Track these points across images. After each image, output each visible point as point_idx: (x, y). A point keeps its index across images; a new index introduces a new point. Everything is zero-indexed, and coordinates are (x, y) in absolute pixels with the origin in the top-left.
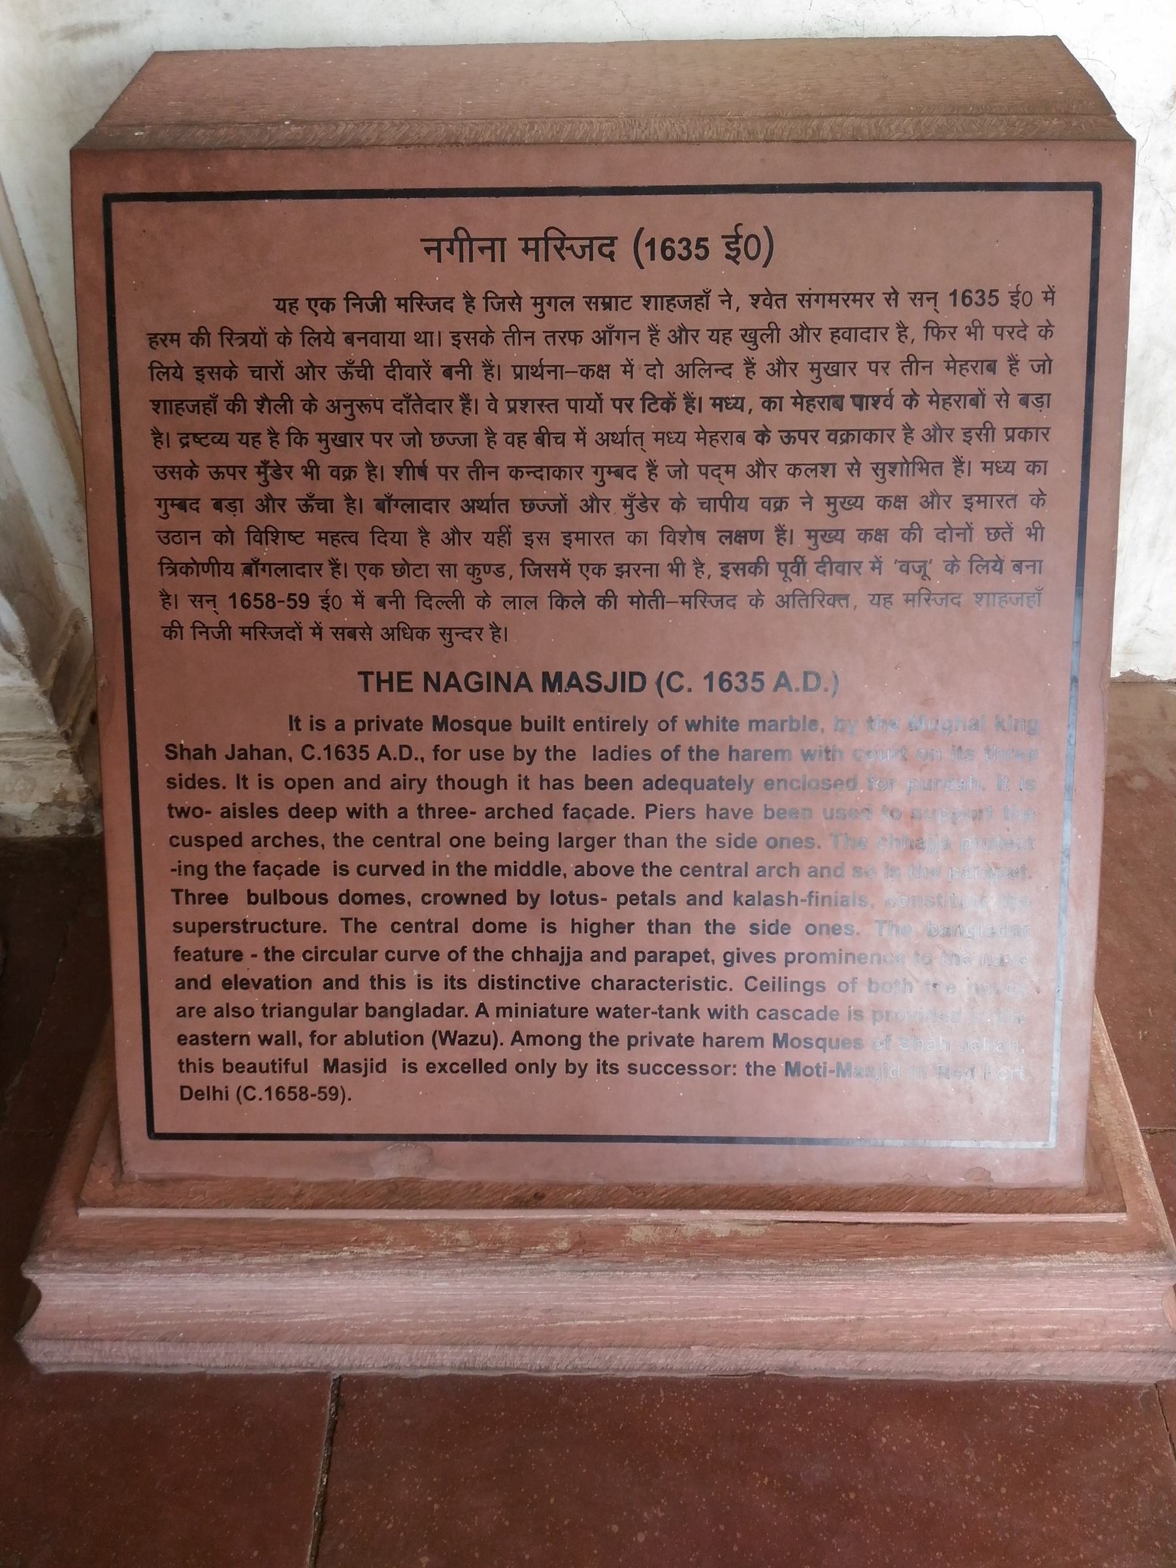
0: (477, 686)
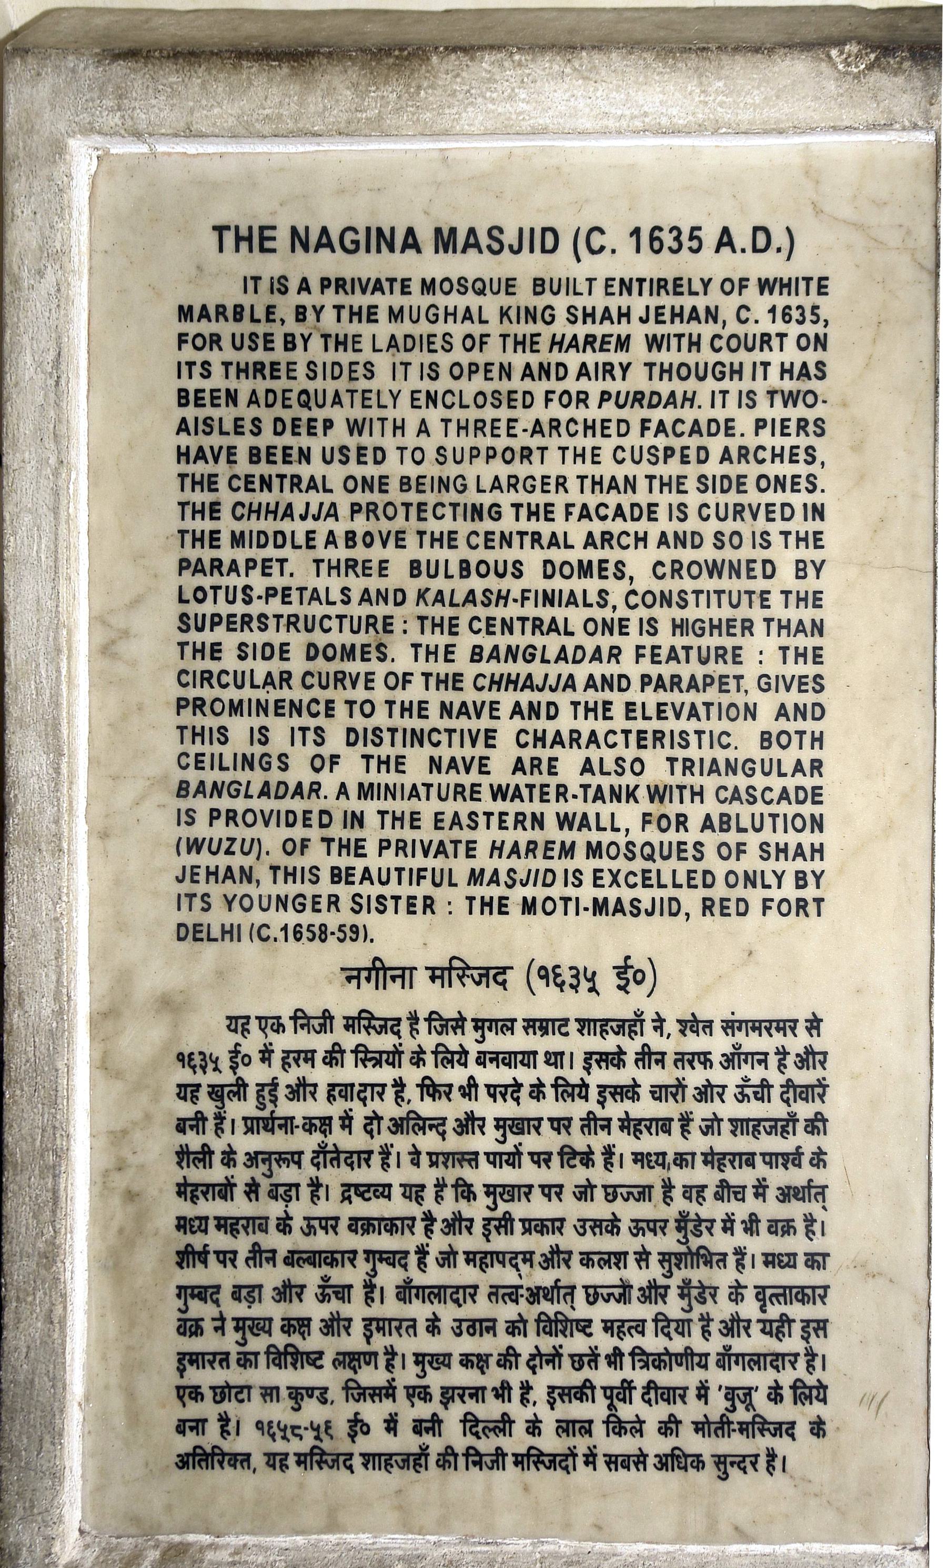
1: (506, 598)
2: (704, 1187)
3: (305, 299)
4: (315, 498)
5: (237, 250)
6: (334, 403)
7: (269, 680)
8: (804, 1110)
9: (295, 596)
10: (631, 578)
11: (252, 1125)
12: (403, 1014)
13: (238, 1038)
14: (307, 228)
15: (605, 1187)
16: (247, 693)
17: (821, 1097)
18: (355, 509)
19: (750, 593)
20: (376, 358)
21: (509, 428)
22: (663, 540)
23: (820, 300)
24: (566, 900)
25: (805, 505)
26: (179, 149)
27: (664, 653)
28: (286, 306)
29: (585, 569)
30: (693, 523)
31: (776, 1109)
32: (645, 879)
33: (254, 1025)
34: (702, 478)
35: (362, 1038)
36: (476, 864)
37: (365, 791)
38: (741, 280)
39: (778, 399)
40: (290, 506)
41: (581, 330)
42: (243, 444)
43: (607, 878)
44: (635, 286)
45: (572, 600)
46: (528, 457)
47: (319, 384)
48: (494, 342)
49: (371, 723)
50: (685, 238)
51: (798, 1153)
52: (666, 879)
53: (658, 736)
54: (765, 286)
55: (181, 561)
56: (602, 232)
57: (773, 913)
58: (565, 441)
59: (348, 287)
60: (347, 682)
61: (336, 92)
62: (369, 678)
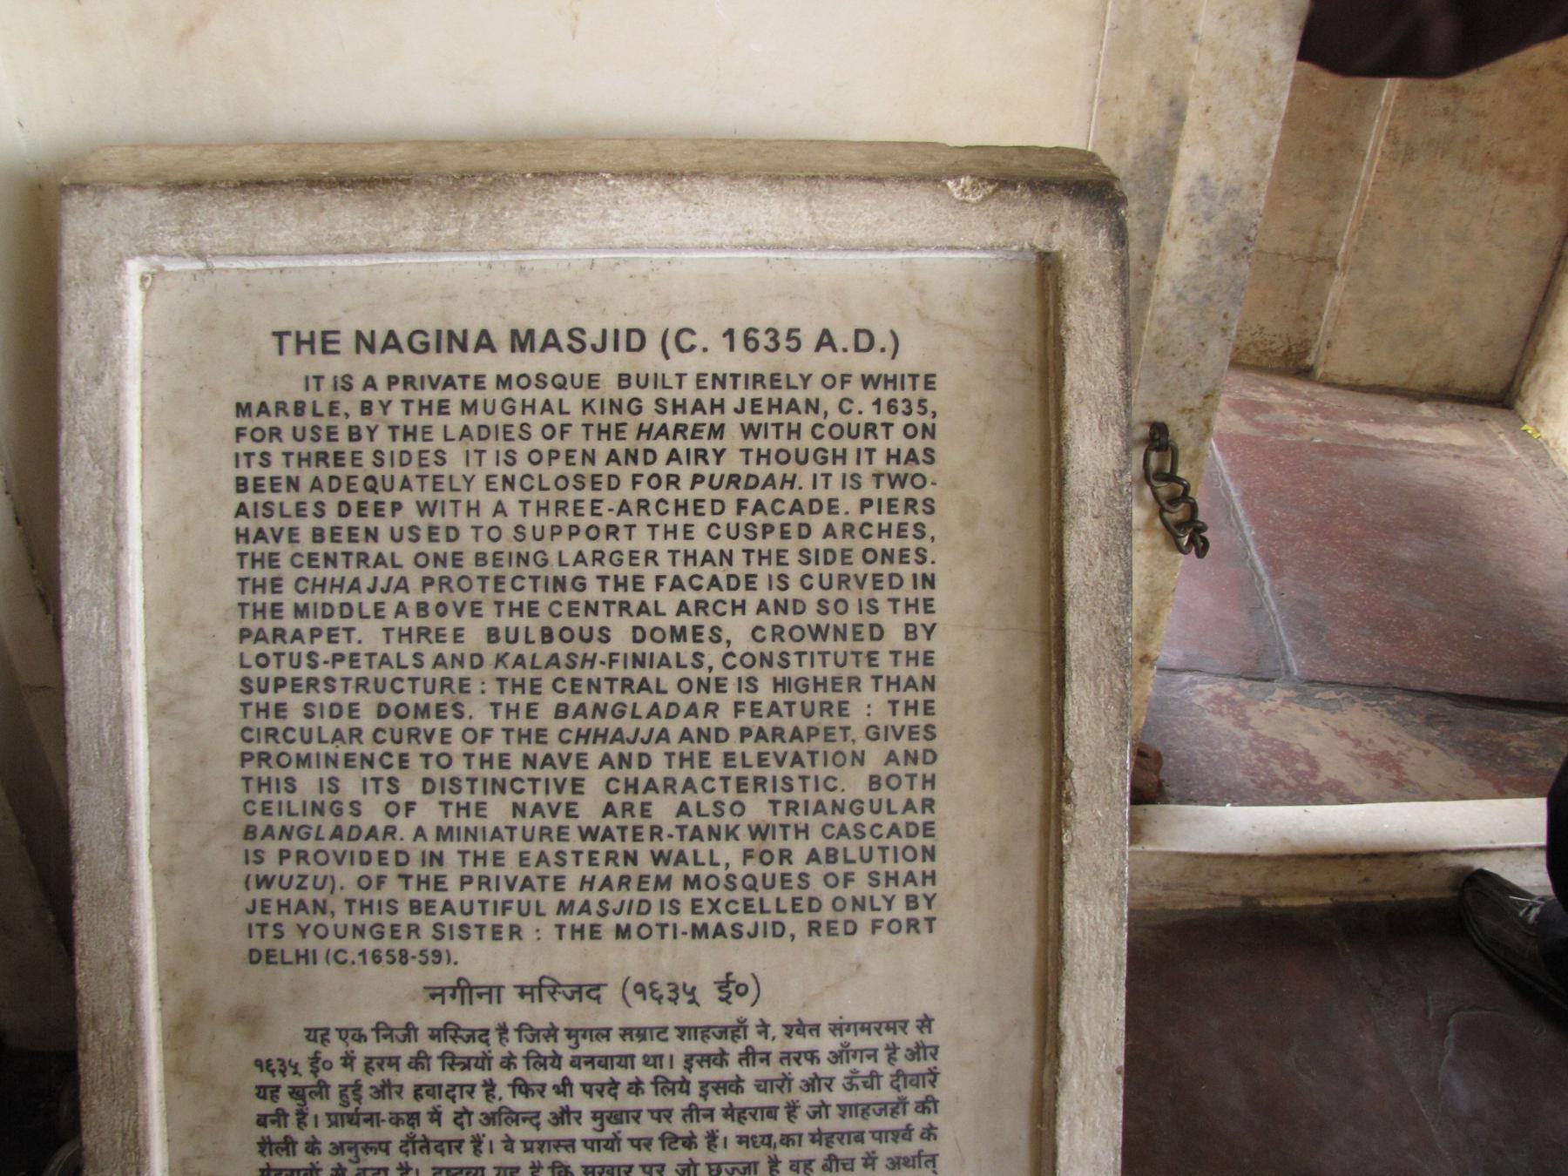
0: (422, 348)
1: (593, 661)
2: (811, 1161)
3: (369, 395)
4: (383, 573)
5: (298, 352)
6: (403, 487)
7: (337, 736)
8: (914, 1095)
9: (364, 660)
10: (729, 642)
11: (335, 1120)
12: (491, 1024)
13: (318, 1046)
14: (373, 332)
15: (709, 1165)
16: (314, 747)
17: (933, 1083)
18: (427, 582)
19: (857, 654)
20: (446, 446)
21: (593, 508)
22: (762, 607)
23: (928, 395)
24: (663, 926)
25: (915, 576)
26: (236, 265)
27: (765, 707)
28: (350, 402)
29: (678, 634)
30: (794, 591)
31: (886, 1094)
32: (746, 906)
33: (334, 1036)
34: (803, 552)
35: (449, 1045)
36: (566, 896)
37: (443, 834)
38: (843, 376)
39: (884, 482)
40: (356, 580)
41: (671, 420)
42: (306, 526)
43: (706, 907)
44: (729, 381)
45: (664, 661)
46: (614, 534)
47: (386, 470)
48: (577, 431)
49: (447, 774)
50: (782, 338)
51: (908, 1130)
52: (770, 904)
53: (760, 782)
54: (867, 381)
55: (242, 630)
56: (692, 332)
57: (883, 934)
58: (654, 518)
59: (417, 383)
60: (422, 737)
61: (414, 218)
62: (445, 735)
